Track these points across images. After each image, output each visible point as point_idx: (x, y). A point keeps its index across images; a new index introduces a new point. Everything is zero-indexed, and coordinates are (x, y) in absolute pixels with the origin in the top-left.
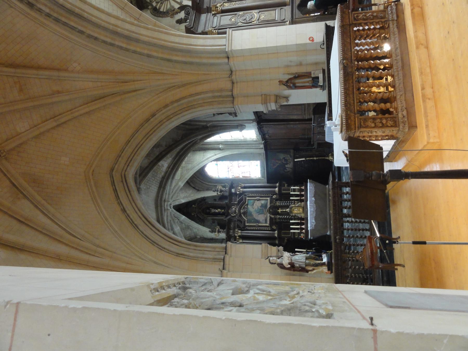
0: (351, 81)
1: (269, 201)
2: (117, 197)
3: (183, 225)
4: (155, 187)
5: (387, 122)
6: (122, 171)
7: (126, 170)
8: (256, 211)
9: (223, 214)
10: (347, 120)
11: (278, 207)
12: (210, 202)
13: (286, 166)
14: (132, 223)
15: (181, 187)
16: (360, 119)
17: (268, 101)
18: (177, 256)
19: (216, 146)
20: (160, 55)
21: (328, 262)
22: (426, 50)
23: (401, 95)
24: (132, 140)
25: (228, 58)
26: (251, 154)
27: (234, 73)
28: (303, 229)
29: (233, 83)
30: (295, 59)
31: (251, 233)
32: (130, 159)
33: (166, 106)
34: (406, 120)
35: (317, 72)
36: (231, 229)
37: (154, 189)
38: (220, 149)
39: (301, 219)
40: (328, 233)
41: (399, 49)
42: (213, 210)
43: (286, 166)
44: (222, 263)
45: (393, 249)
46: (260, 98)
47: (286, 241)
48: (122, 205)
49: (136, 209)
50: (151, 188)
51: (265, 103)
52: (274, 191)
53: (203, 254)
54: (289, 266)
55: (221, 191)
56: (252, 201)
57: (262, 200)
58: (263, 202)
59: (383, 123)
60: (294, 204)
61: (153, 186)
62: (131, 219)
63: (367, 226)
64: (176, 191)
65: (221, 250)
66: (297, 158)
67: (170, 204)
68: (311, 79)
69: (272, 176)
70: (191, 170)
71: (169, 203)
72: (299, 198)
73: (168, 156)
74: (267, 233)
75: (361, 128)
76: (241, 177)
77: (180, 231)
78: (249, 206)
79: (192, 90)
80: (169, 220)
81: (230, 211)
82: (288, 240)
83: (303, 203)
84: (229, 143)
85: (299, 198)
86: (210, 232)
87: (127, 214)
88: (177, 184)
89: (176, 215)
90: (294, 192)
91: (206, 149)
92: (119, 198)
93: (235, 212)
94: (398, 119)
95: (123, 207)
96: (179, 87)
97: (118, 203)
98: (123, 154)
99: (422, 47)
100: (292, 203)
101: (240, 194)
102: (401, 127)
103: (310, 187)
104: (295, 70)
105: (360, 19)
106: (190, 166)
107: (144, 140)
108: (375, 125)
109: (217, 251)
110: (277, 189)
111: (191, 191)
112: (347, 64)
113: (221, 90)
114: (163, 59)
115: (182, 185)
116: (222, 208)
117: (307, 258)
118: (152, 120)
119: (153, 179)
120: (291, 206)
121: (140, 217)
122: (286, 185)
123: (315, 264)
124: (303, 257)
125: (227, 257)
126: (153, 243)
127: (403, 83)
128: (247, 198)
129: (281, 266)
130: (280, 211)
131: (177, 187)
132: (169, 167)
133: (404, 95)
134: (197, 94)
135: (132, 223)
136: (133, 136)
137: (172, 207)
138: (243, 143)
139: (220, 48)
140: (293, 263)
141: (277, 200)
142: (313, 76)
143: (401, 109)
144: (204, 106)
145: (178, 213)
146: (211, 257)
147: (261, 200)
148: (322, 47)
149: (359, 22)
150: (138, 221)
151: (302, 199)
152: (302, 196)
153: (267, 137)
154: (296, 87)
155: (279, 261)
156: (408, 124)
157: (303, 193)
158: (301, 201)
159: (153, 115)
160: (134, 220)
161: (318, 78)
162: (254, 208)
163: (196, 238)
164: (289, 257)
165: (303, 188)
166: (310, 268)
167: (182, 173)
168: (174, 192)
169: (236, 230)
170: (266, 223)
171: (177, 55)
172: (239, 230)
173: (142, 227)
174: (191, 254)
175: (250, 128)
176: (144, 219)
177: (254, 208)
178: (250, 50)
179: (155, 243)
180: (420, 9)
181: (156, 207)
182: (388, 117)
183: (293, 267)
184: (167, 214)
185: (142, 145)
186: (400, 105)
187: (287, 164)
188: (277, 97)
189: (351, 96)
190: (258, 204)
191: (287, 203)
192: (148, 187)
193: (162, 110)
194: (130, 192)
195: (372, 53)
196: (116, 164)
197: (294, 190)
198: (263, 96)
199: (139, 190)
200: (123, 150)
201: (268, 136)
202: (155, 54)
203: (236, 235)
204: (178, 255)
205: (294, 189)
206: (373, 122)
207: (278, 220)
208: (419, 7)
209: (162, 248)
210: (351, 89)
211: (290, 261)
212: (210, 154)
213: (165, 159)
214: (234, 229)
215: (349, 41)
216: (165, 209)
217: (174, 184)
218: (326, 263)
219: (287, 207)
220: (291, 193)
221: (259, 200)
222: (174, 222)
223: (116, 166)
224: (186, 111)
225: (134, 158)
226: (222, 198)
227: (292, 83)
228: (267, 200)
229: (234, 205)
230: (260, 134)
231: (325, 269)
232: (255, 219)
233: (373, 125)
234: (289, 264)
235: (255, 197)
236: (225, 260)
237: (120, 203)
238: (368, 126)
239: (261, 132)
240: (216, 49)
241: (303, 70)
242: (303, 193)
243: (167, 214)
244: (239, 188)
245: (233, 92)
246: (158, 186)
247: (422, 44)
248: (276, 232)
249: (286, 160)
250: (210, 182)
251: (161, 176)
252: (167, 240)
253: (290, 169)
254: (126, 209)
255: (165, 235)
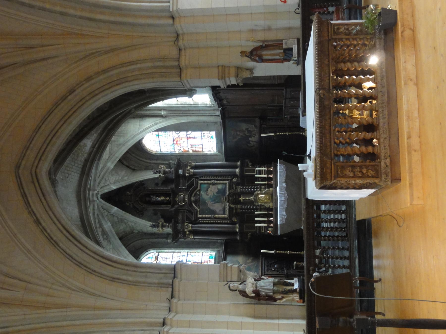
0: (327, 117)
1: (228, 185)
2: (27, 204)
3: (116, 218)
4: (76, 174)
5: (367, 171)
6: (32, 168)
7: (37, 167)
8: (210, 198)
9: (168, 203)
10: (322, 169)
11: (240, 195)
12: (151, 187)
13: (250, 139)
14: (50, 238)
15: (109, 171)
16: (337, 166)
17: (227, 76)
18: (111, 281)
19: (156, 112)
20: (79, 13)
21: (300, 289)
22: (415, 87)
23: (385, 138)
24: (43, 126)
25: (173, 18)
26: (204, 122)
27: (181, 37)
28: (271, 222)
29: (180, 50)
30: (262, 23)
31: (205, 227)
32: (41, 152)
33: (89, 79)
34: (389, 170)
35: (290, 41)
36: (178, 223)
37: (75, 177)
38: (161, 116)
39: (269, 209)
40: (302, 228)
41: (385, 78)
42: (154, 199)
43: (250, 139)
44: (170, 290)
45: (374, 289)
46: (215, 71)
47: (249, 236)
48: (35, 215)
49: (55, 219)
50: (70, 176)
51: (222, 79)
52: (235, 172)
53: (146, 276)
54: (254, 295)
55: (165, 173)
56: (206, 186)
57: (219, 184)
58: (220, 187)
59: (363, 173)
60: (260, 190)
61: (73, 174)
62: (48, 234)
63: (347, 245)
64: (105, 174)
65: (170, 272)
66: (264, 133)
67: (97, 194)
68: (282, 51)
69: (232, 150)
70: (124, 145)
71: (96, 192)
72: (266, 182)
73: (93, 132)
74: (226, 227)
75: (337, 177)
76: (191, 151)
77: (111, 228)
78: (201, 192)
79: (125, 57)
80: (96, 216)
81: (177, 199)
82: (252, 235)
83: (271, 189)
84: (175, 109)
85: (266, 182)
86: (151, 226)
87: (43, 227)
88: (105, 165)
89: (105, 207)
90: (260, 174)
91: (143, 117)
92: (30, 206)
93: (184, 200)
94: (381, 168)
95: (37, 218)
96: (106, 52)
97: (29, 213)
98: (32, 145)
99: (411, 84)
100: (257, 188)
101: (191, 177)
102: (383, 179)
103: (280, 169)
104: (262, 36)
105: (341, 33)
106: (121, 140)
107: (59, 126)
108: (354, 175)
109: (162, 273)
110: (238, 170)
111: (124, 172)
112: (324, 95)
113: (164, 59)
114: (81, 17)
115: (112, 167)
116: (166, 194)
117: (275, 284)
118: (70, 97)
119: (73, 163)
120: (256, 192)
121: (60, 230)
122: (250, 164)
123: (285, 291)
124: (271, 282)
125: (177, 281)
126: (80, 264)
127: (388, 123)
128: (199, 182)
129: (243, 293)
130: (242, 199)
131: (104, 171)
132: (93, 147)
133: (388, 138)
134: (131, 63)
135: (50, 238)
136: (44, 119)
137: (99, 196)
138: (194, 109)
139: (162, 6)
140: (259, 291)
141: (238, 184)
142: (284, 46)
143: (385, 156)
144: (141, 79)
145: (108, 204)
146: (156, 281)
147: (217, 184)
148: (297, 11)
149: (340, 37)
150: (58, 236)
151: (270, 184)
152: (270, 179)
153: (225, 102)
154: (262, 60)
155: (241, 287)
156: (392, 177)
157: (271, 176)
158: (270, 186)
159: (72, 91)
160: (52, 236)
161: (291, 49)
162: (208, 195)
163: (133, 233)
164: (253, 284)
165: (272, 169)
166: (279, 296)
167: (111, 150)
168: (101, 176)
169: (186, 224)
170: (224, 214)
171: (101, 13)
172: (189, 223)
173: (65, 244)
174: (131, 279)
175: (203, 93)
176: (65, 232)
177: (208, 195)
178: (202, 10)
179: (82, 264)
180: (411, 32)
181: (79, 201)
182: (369, 165)
183: (258, 296)
184: (94, 206)
185: (57, 131)
186: (383, 151)
187: (251, 136)
188: (238, 69)
189: (328, 136)
190: (213, 190)
191: (251, 188)
192: (67, 175)
193: (83, 84)
194: (44, 196)
195: (354, 79)
196: (23, 159)
197: (260, 172)
198: (220, 68)
199: (54, 183)
200: (31, 140)
201: (227, 101)
202: (71, 11)
203: (185, 230)
204: (113, 279)
205: (260, 170)
206: (352, 171)
207: (239, 211)
208: (410, 29)
209: (92, 272)
210: (327, 127)
211: (255, 289)
212: (148, 123)
213: (88, 136)
214: (183, 222)
215: (327, 63)
216: (90, 201)
217: (101, 165)
218: (298, 290)
219: (251, 194)
220: (256, 176)
221: (213, 184)
222: (103, 217)
223: (24, 163)
224: (117, 85)
225: (48, 149)
226: (166, 181)
227: (256, 54)
228: (226, 184)
229: (182, 190)
230: (215, 101)
231: (296, 297)
232: (210, 209)
233: (352, 175)
234: (254, 292)
235: (210, 180)
236: (174, 285)
237: (32, 213)
238: (346, 175)
239: (217, 98)
240: (156, 6)
241: (271, 36)
242: (271, 176)
243: (94, 206)
244: (189, 168)
245: (180, 61)
246: (79, 172)
247: (411, 80)
248: (237, 225)
249: (250, 132)
250: (149, 159)
251: (83, 159)
252: (98, 260)
253: (255, 143)
254: (41, 221)
255: (95, 253)
